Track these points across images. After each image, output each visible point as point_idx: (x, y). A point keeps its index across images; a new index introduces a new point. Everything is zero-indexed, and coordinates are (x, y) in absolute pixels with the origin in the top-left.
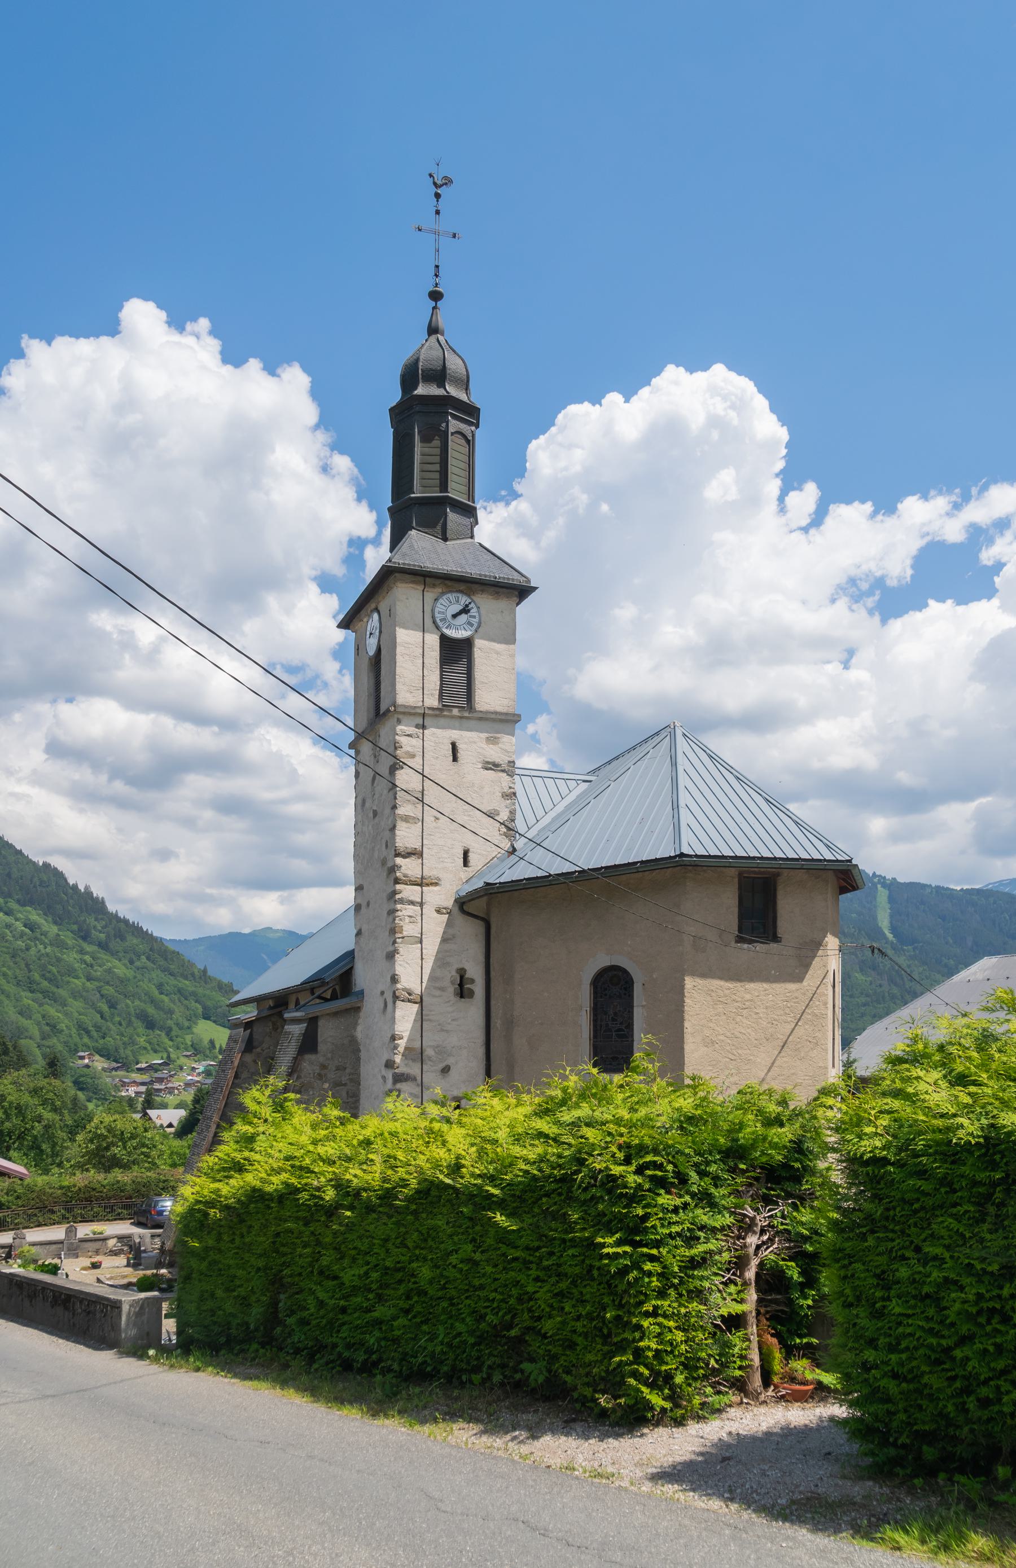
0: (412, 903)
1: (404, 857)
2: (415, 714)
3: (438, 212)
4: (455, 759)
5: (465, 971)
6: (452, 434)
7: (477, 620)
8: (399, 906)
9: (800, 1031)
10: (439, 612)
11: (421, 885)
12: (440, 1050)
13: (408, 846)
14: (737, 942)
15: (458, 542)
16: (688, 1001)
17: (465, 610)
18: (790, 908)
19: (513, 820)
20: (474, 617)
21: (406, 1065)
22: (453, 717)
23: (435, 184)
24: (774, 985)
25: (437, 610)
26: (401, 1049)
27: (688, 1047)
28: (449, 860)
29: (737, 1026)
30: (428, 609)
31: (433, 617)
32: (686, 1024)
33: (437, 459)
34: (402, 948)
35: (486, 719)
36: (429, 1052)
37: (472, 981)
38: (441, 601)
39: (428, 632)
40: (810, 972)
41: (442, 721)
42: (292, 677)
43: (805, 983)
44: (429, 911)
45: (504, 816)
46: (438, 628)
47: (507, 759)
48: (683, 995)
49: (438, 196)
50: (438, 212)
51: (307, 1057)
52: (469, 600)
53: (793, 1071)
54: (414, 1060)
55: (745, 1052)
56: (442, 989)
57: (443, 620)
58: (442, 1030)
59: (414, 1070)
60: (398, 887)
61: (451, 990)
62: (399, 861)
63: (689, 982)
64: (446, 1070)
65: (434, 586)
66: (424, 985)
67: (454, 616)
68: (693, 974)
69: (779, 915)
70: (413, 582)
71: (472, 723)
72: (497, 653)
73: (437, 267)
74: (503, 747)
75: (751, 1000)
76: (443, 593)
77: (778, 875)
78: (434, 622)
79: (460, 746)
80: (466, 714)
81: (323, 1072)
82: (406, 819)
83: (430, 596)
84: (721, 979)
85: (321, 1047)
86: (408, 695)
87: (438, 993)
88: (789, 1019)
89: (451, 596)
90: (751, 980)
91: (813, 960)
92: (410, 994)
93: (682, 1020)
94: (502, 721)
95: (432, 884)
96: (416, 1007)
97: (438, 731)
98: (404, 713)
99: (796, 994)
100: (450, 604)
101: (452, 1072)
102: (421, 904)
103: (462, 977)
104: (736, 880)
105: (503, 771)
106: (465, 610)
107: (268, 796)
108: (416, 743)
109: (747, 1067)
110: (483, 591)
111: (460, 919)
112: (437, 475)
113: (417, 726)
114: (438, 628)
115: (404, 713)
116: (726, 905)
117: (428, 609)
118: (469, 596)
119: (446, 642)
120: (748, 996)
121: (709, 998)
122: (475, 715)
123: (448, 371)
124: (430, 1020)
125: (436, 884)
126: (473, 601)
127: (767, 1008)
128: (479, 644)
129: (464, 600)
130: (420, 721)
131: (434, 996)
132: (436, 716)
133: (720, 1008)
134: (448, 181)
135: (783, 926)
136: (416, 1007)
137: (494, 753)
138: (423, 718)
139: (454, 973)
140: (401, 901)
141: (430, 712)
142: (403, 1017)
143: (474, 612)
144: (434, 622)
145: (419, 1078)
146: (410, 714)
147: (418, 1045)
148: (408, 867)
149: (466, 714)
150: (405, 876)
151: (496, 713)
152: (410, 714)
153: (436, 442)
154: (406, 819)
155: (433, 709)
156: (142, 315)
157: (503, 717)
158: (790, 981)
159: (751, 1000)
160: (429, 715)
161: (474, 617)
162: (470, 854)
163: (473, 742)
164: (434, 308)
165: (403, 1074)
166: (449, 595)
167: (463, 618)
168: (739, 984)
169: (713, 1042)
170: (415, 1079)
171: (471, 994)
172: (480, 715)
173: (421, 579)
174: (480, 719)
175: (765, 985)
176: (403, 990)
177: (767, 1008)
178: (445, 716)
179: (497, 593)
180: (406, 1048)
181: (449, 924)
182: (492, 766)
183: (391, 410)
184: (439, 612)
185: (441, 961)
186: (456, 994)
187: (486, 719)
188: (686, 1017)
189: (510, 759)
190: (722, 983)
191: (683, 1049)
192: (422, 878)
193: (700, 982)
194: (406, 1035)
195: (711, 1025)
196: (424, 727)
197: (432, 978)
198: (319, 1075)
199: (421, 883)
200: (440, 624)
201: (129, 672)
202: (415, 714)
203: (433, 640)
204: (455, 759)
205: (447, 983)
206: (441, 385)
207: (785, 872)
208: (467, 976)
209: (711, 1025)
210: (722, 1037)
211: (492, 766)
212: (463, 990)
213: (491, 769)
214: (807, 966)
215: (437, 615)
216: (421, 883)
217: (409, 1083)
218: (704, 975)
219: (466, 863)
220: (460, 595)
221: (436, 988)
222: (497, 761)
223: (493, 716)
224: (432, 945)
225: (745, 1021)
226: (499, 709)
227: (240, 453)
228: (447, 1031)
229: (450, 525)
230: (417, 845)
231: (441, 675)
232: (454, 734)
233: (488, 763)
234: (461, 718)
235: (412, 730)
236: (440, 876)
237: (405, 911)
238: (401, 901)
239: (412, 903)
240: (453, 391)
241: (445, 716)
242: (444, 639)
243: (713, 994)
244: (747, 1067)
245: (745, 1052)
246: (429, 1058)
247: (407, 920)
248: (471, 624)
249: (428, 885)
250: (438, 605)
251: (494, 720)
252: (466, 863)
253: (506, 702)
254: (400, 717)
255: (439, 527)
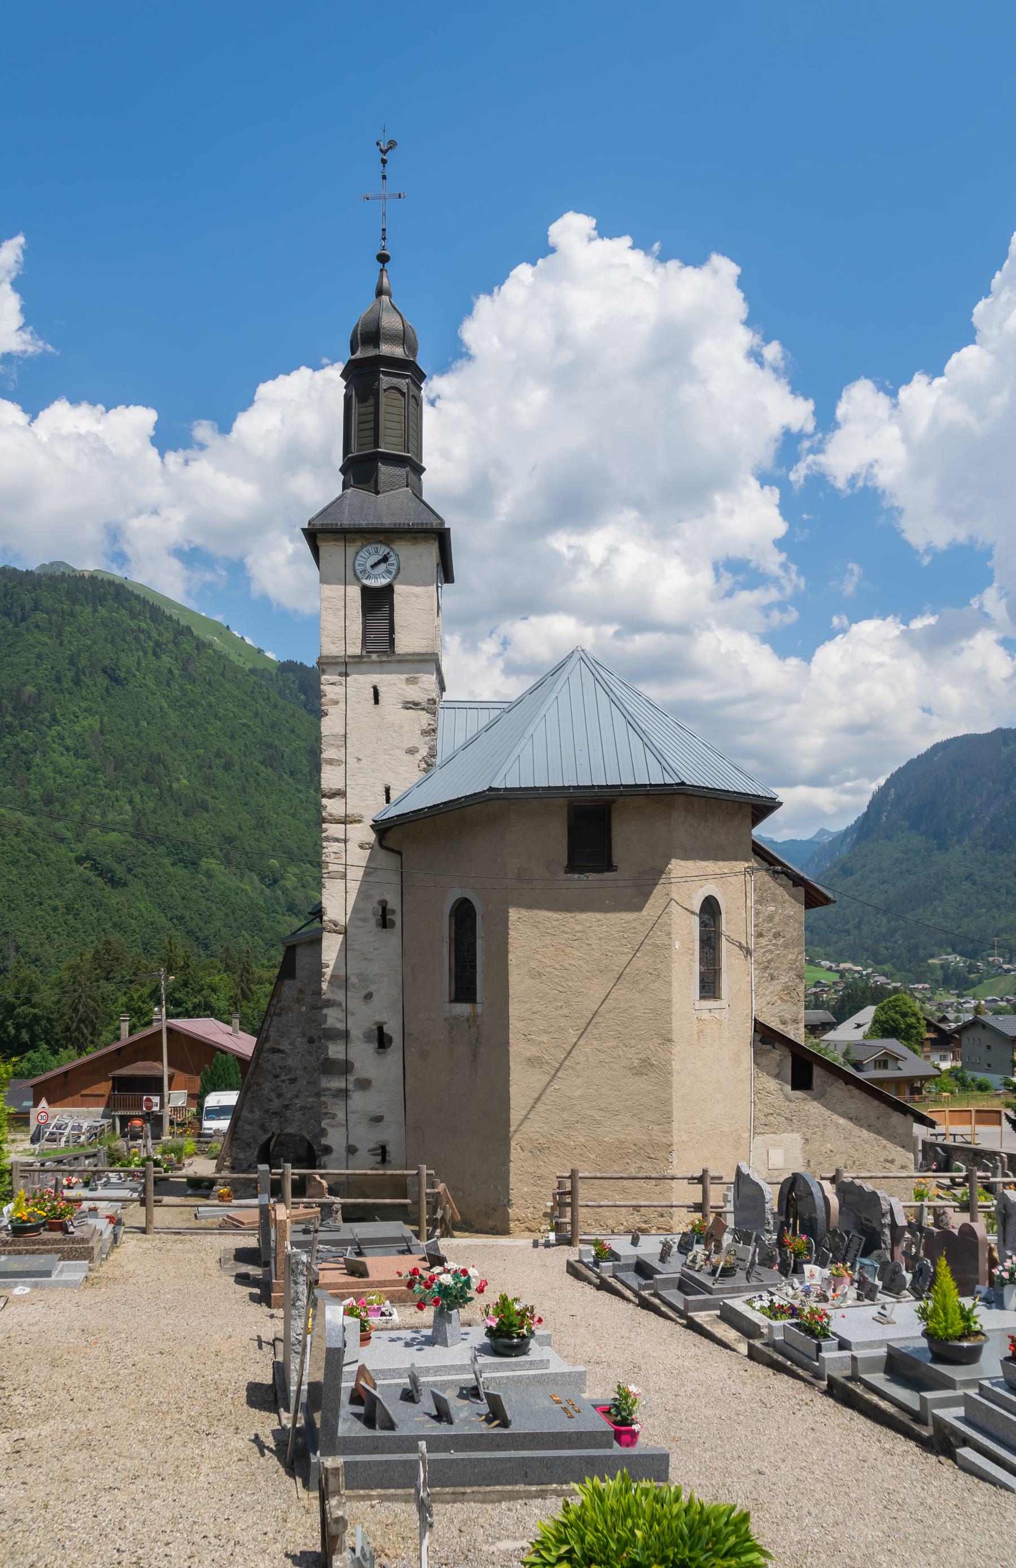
0: (337, 840)
1: (330, 797)
2: (338, 663)
3: (384, 177)
4: (377, 701)
5: (386, 902)
6: (385, 390)
7: (395, 567)
8: (325, 844)
9: (639, 963)
10: (359, 565)
11: (345, 823)
12: (362, 977)
13: (333, 787)
14: (566, 872)
15: (392, 492)
16: (512, 933)
17: (385, 559)
18: (626, 836)
19: (434, 756)
20: (393, 565)
21: (332, 992)
22: (373, 662)
23: (381, 151)
24: (608, 915)
25: (357, 562)
26: (327, 977)
27: (513, 979)
28: (371, 798)
29: (566, 958)
30: (349, 562)
31: (354, 570)
32: (511, 956)
33: (372, 417)
34: (327, 882)
35: (407, 661)
36: (353, 979)
37: (393, 912)
38: (361, 554)
39: (350, 584)
40: (650, 901)
41: (363, 667)
42: (737, 572)
43: (644, 912)
44: (353, 846)
45: (424, 751)
46: (358, 579)
47: (426, 697)
48: (507, 928)
49: (384, 162)
50: (384, 177)
51: (287, 982)
52: (387, 550)
53: (631, 1004)
54: (338, 987)
55: (576, 984)
56: (365, 920)
57: (363, 571)
58: (365, 959)
59: (339, 996)
60: (324, 826)
61: (373, 921)
62: (325, 801)
63: (513, 914)
64: (369, 996)
65: (354, 540)
66: (348, 916)
67: (372, 567)
68: (518, 905)
69: (613, 843)
70: (335, 540)
71: (393, 666)
72: (416, 596)
73: (384, 230)
74: (423, 686)
75: (582, 932)
76: (363, 546)
77: (613, 802)
78: (355, 575)
79: (380, 689)
80: (385, 659)
81: (301, 996)
82: (331, 762)
83: (351, 550)
84: (549, 909)
85: (299, 973)
86: (332, 646)
87: (361, 924)
88: (626, 950)
89: (371, 548)
90: (583, 910)
91: (654, 888)
92: (336, 926)
93: (506, 952)
94: (420, 661)
95: (355, 821)
96: (340, 938)
97: (360, 677)
98: (327, 664)
99: (634, 925)
100: (369, 555)
101: (375, 998)
102: (345, 841)
103: (384, 909)
104: (565, 810)
105: (423, 709)
106: (385, 559)
107: (709, 697)
108: (339, 690)
109: (578, 999)
110: (400, 539)
111: (381, 853)
112: (371, 433)
113: (340, 675)
114: (358, 579)
115: (327, 664)
116: (555, 836)
117: (349, 562)
118: (388, 545)
119: (367, 592)
120: (579, 928)
121: (536, 930)
122: (393, 658)
123: (382, 331)
124: (353, 950)
125: (360, 821)
126: (392, 550)
127: (600, 939)
128: (398, 588)
129: (383, 550)
130: (342, 669)
131: (357, 927)
132: (358, 663)
133: (548, 940)
134: (392, 145)
135: (616, 860)
136: (340, 938)
137: (414, 693)
138: (345, 665)
139: (376, 905)
140: (327, 839)
141: (351, 660)
142: (329, 947)
143: (392, 560)
144: (355, 575)
145: (344, 1005)
146: (333, 664)
147: (342, 973)
148: (333, 807)
149: (385, 659)
150: (331, 815)
151: (414, 654)
152: (333, 664)
153: (371, 401)
154: (331, 762)
155: (353, 657)
156: (571, 230)
157: (420, 658)
158: (626, 911)
159: (582, 932)
160: (351, 663)
161: (393, 565)
162: (391, 791)
163: (394, 684)
164: (382, 270)
165: (329, 1000)
166: (369, 547)
167: (383, 566)
168: (569, 915)
169: (540, 974)
170: (340, 1005)
171: (393, 924)
172: (399, 658)
173: (342, 535)
174: (399, 661)
175: (599, 916)
176: (330, 921)
177: (600, 939)
178: (365, 662)
179: (415, 538)
180: (332, 976)
181: (371, 859)
182: (412, 705)
183: (341, 376)
184: (359, 565)
185: (363, 894)
186: (378, 925)
187: (407, 661)
188: (510, 949)
189: (430, 697)
190: (550, 914)
191: (508, 981)
192: (346, 816)
193: (525, 913)
194: (332, 964)
195: (538, 956)
196: (346, 675)
197: (355, 910)
198: (298, 999)
199: (346, 820)
200: (360, 576)
201: (584, 584)
202: (338, 663)
203: (354, 592)
204: (377, 701)
205: (369, 914)
206: (377, 346)
207: (621, 799)
208: (388, 907)
209: (538, 956)
210: (548, 969)
211: (412, 705)
212: (385, 921)
213: (411, 708)
214: (647, 895)
215: (357, 567)
216: (346, 820)
217: (335, 1009)
218: (530, 907)
219: (388, 800)
220: (379, 546)
221: (358, 919)
222: (417, 700)
223: (410, 658)
224: (356, 875)
225: (575, 952)
226: (418, 650)
227: (670, 351)
228: (370, 960)
229: (382, 478)
230: (341, 786)
231: (364, 623)
232: (375, 678)
233: (408, 702)
234: (381, 662)
235: (336, 678)
236: (363, 814)
237: (331, 849)
238: (327, 839)
239: (337, 840)
240: (386, 349)
241: (365, 662)
242: (365, 590)
243: (540, 926)
244: (578, 999)
245: (576, 984)
246: (353, 985)
247: (333, 856)
248: (389, 572)
249: (351, 823)
250: (359, 558)
251: (413, 661)
252: (388, 800)
253: (424, 643)
254: (325, 667)
255: (372, 482)
